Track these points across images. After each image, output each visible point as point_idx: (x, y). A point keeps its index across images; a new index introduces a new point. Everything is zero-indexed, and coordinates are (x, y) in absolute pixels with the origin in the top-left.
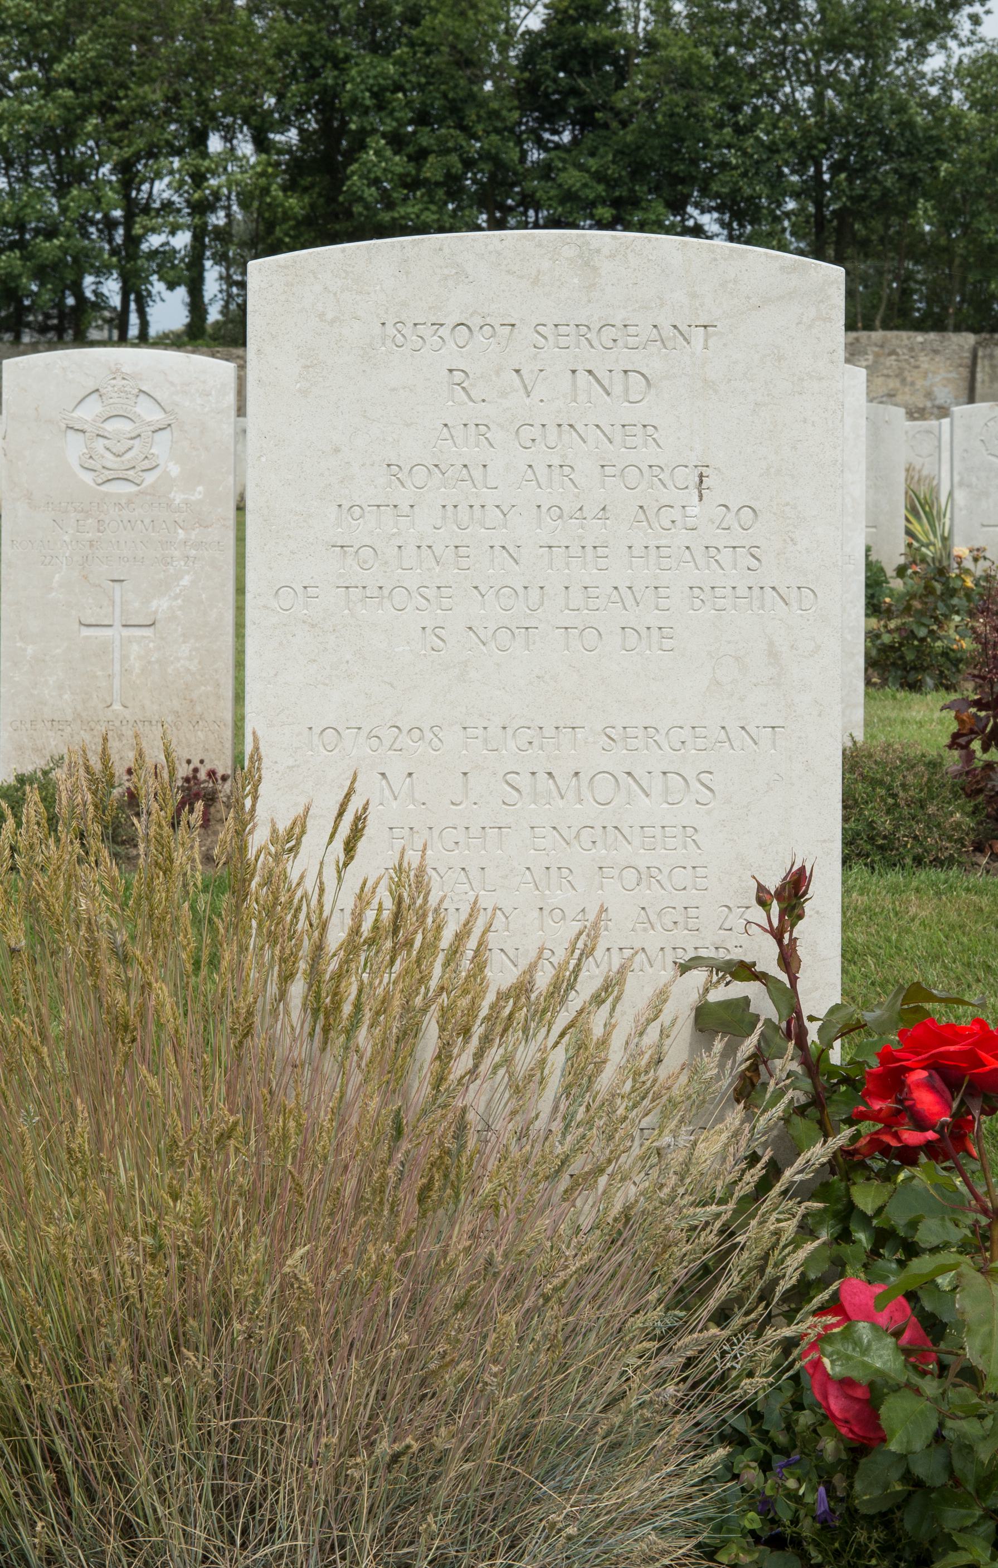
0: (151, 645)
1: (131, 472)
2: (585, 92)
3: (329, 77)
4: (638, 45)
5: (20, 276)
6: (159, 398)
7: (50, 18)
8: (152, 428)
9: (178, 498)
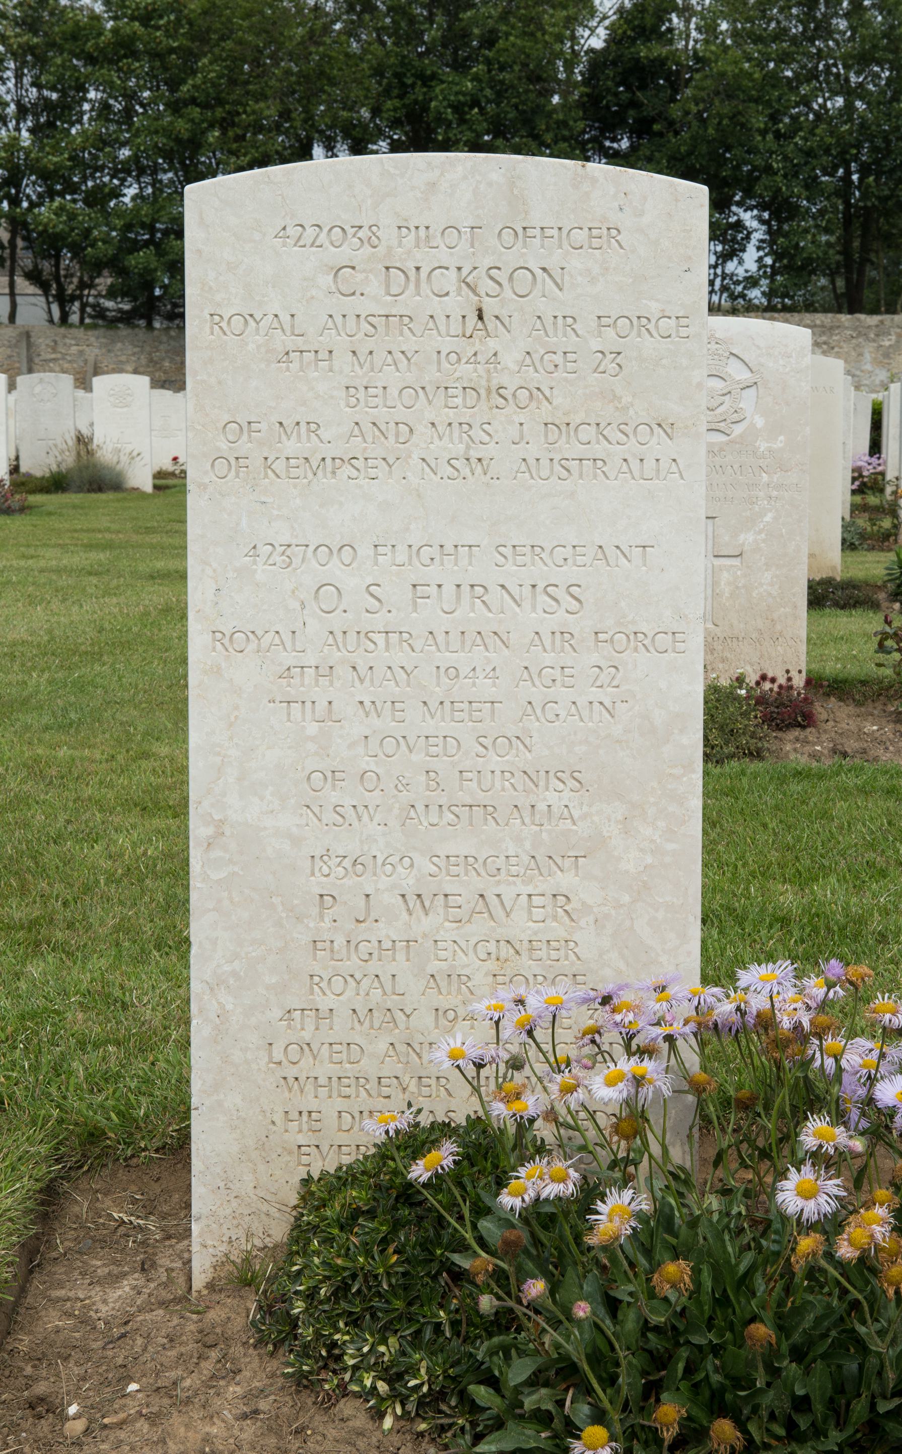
0: (739, 573)
1: (722, 424)
2: (642, 104)
3: (419, 93)
4: (687, 59)
5: (156, 270)
6: (746, 360)
7: (176, 44)
8: (741, 386)
9: (763, 446)
